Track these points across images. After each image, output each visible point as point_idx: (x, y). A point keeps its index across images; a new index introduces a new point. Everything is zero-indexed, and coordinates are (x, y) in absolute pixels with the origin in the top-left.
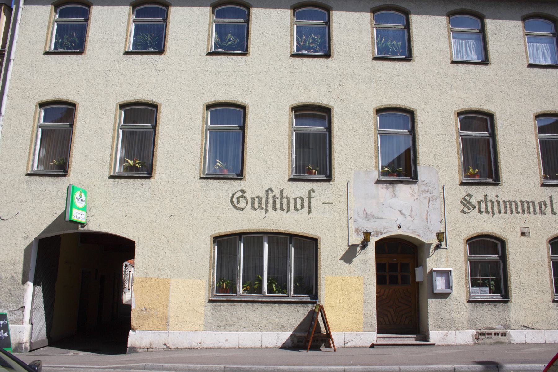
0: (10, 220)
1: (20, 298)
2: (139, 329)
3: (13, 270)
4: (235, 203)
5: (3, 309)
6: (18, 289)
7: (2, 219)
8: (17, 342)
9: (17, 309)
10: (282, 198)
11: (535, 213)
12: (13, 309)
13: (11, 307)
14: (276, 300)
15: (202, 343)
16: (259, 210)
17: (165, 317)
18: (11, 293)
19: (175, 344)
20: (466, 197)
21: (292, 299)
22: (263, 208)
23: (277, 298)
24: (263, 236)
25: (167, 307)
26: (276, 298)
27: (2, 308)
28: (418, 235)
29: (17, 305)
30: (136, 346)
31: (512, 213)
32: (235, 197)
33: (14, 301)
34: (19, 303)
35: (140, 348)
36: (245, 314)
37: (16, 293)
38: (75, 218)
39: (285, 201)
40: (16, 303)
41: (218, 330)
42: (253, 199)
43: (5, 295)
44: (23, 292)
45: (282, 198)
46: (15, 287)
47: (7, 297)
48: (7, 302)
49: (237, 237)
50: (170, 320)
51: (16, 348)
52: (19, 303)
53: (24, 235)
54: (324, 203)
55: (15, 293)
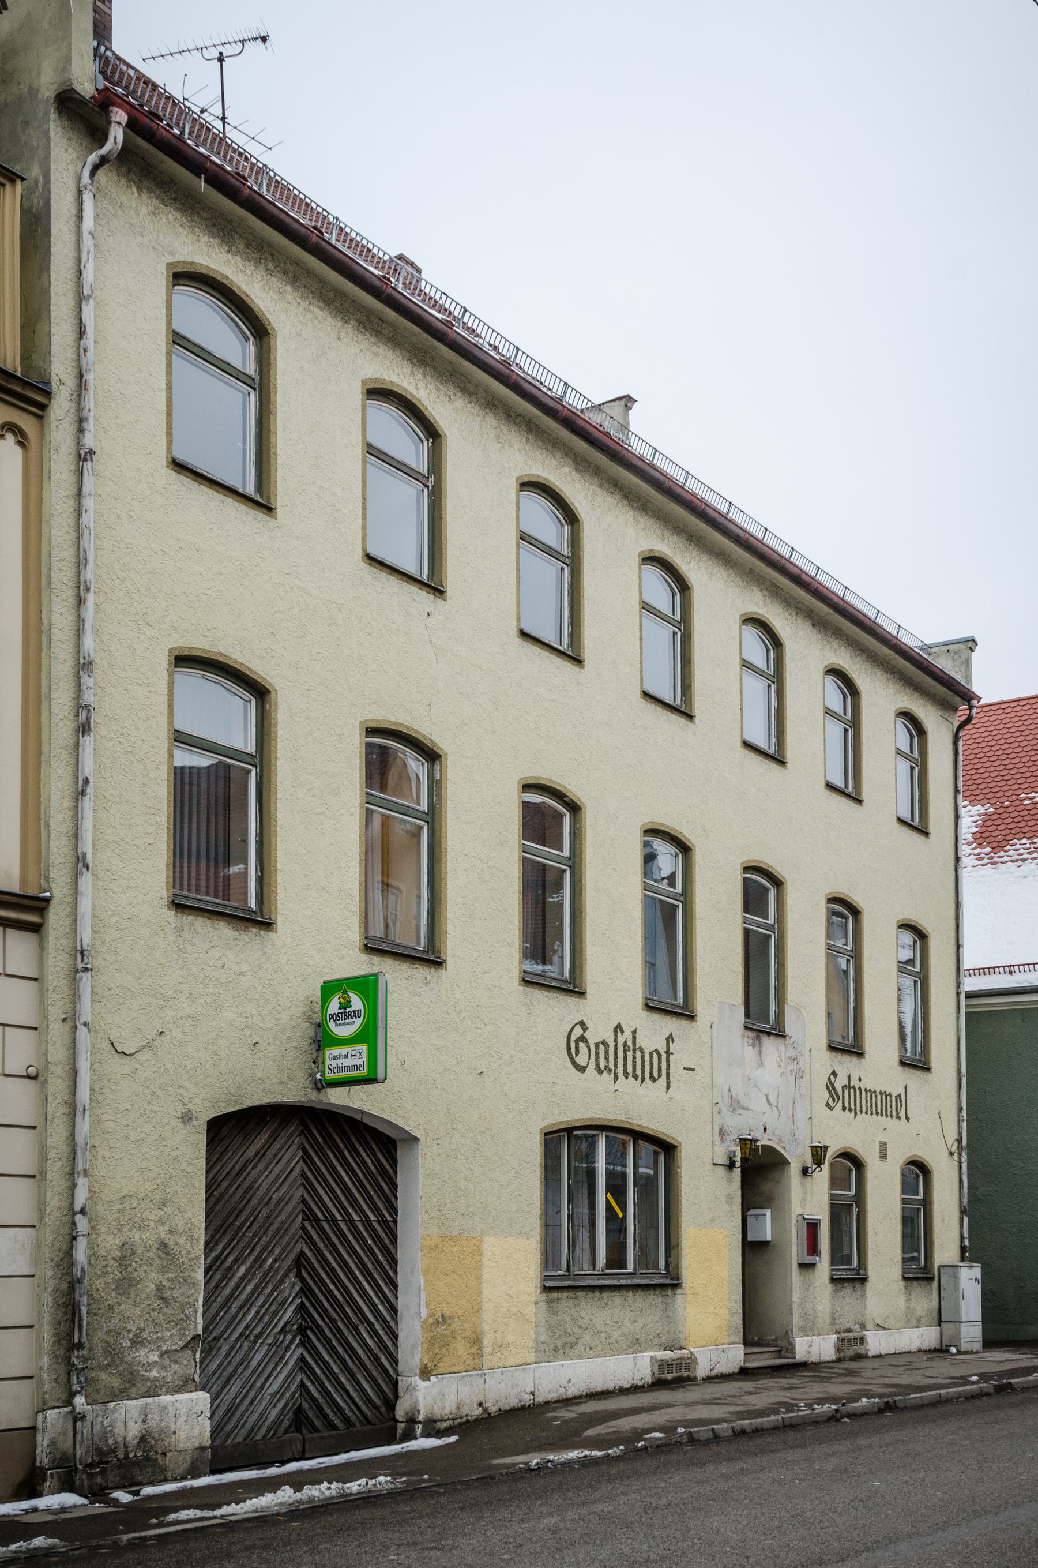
0: (139, 1056)
1: (187, 1311)
2: (434, 1373)
3: (160, 1222)
4: (574, 1054)
5: (146, 1350)
6: (179, 1281)
7: (119, 1050)
8: (197, 1445)
9: (181, 1344)
10: (634, 1050)
11: (892, 1117)
12: (174, 1348)
13: (166, 1340)
14: (623, 1282)
15: (537, 1393)
16: (605, 1073)
17: (475, 1337)
18: (165, 1296)
19: (497, 1401)
20: (242, 866)
21: (641, 1279)
22: (610, 1071)
23: (626, 1278)
24: (594, 1136)
25: (478, 1311)
26: (623, 1278)
27: (145, 1346)
28: (784, 1148)
29: (182, 1332)
30: (435, 1417)
31: (872, 1113)
32: (573, 1038)
33: (173, 1321)
34: (185, 1325)
35: (442, 1420)
36: (592, 1317)
37: (176, 1294)
38: (332, 1074)
39: (638, 1054)
40: (178, 1327)
41: (555, 1358)
42: (597, 1046)
43: (149, 1302)
44: (193, 1291)
45: (634, 1050)
46: (172, 1275)
47: (154, 1310)
48: (156, 1324)
49: (564, 1136)
50: (486, 1342)
51: (193, 1463)
52: (185, 1325)
53: (180, 1109)
54: (685, 1069)
55: (175, 1296)
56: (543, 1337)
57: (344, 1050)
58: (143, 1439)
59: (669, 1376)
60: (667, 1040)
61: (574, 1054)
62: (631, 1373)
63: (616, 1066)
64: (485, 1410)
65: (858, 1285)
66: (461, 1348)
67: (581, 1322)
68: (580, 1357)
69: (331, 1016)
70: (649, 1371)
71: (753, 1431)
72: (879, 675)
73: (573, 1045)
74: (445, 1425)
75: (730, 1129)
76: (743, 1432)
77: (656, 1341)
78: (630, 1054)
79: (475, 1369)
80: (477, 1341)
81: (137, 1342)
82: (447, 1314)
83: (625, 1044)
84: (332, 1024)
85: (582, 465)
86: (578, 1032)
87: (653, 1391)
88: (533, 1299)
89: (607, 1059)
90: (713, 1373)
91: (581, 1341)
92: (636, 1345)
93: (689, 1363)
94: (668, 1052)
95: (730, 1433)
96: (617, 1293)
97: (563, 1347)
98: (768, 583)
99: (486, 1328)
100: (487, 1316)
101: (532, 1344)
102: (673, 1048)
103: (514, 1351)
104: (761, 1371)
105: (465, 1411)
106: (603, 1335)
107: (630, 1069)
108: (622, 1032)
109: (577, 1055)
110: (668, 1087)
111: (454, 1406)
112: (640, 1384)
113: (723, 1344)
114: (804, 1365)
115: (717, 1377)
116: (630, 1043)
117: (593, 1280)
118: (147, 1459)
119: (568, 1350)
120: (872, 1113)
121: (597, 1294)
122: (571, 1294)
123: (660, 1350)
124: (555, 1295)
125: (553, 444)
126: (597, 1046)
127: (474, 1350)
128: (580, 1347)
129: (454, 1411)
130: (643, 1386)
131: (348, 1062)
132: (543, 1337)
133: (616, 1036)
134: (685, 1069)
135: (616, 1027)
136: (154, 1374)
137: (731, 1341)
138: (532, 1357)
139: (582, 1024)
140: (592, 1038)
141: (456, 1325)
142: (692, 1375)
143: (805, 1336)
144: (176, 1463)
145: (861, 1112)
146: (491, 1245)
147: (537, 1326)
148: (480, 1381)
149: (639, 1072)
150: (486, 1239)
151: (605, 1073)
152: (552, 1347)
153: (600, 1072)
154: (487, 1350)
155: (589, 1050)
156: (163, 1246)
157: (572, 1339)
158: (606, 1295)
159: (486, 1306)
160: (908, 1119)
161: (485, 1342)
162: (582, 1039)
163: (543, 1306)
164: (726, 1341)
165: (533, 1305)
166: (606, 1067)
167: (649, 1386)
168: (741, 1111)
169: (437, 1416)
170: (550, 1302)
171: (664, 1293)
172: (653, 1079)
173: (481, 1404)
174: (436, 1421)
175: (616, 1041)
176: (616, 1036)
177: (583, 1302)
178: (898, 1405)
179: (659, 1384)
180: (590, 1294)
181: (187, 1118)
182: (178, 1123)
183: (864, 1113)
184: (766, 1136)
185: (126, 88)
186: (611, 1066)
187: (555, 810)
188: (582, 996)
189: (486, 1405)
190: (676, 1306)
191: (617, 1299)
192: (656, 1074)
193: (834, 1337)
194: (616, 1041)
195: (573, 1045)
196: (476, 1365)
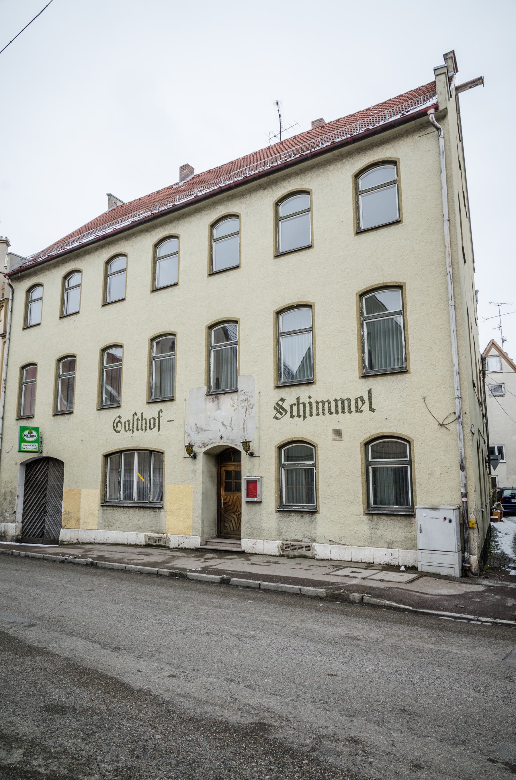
3: (10, 486)
10: (142, 420)
16: (128, 431)
22: (130, 430)
28: (236, 445)
35: (65, 542)
54: (168, 421)
56: (101, 521)
57: (29, 444)
58: (4, 532)
59: (154, 544)
60: (133, 415)
61: (115, 427)
62: (135, 539)
63: (133, 428)
64: (78, 541)
65: (307, 517)
66: (73, 521)
67: (115, 518)
68: (114, 530)
69: (25, 435)
70: (144, 540)
71: (32, 557)
72: (169, 228)
73: (115, 425)
74: (66, 543)
75: (196, 441)
76: (28, 556)
77: (150, 529)
78: (140, 423)
79: (77, 529)
80: (78, 520)
81: (6, 511)
82: (70, 511)
83: (138, 419)
84: (25, 437)
85: (162, 224)
86: (118, 419)
87: (144, 548)
88: (97, 509)
89: (129, 426)
90: (180, 547)
91: (115, 525)
92: (139, 529)
93: (166, 540)
94: (159, 417)
95: (24, 555)
96: (131, 509)
97: (108, 526)
98: (226, 199)
99: (81, 517)
100: (82, 513)
101: (96, 523)
102: (161, 414)
103: (90, 525)
104: (203, 550)
105: (72, 540)
106: (124, 524)
107: (139, 427)
108: (136, 415)
109: (117, 427)
110: (159, 430)
111: (69, 538)
112: (139, 544)
113: (189, 535)
114: (243, 552)
115: (182, 548)
116: (140, 418)
117: (127, 504)
118: (5, 536)
119: (110, 527)
120: (324, 414)
121: (122, 509)
122: (111, 508)
123: (152, 533)
124: (105, 508)
125: (155, 227)
126: (125, 423)
127: (77, 523)
128: (115, 527)
129: (69, 540)
130: (141, 545)
131: (31, 447)
132: (101, 521)
133: (134, 417)
134: (168, 421)
135: (159, 411)
136: (8, 518)
137: (193, 534)
138: (96, 527)
139: (120, 417)
140: (123, 420)
141: (72, 515)
142: (167, 545)
143: (251, 538)
144: (9, 538)
145: (311, 415)
146: (84, 492)
147: (98, 518)
148: (77, 532)
149: (144, 428)
150: (83, 490)
151: (128, 431)
152: (104, 525)
153: (126, 431)
154: (81, 523)
155: (122, 425)
156: (11, 491)
157: (112, 524)
158: (126, 509)
159: (81, 510)
160: (372, 409)
161: (81, 521)
162: (119, 422)
163: (101, 511)
164: (191, 534)
165: (97, 511)
166: (129, 429)
167: (144, 546)
168: (203, 432)
169: (64, 540)
170: (104, 510)
171: (154, 511)
172: (150, 428)
173: (77, 539)
174: (63, 541)
175: (133, 419)
176: (134, 417)
177: (116, 511)
178: (98, 565)
179: (148, 546)
180: (119, 509)
181: (16, 464)
182: (14, 465)
183: (140, 431)
184: (222, 441)
185: (308, 149)
186: (131, 428)
187: (73, 360)
188: (407, 372)
189: (79, 540)
190: (161, 516)
191: (131, 511)
192: (152, 427)
193: (279, 543)
194: (133, 419)
195: (115, 425)
196: (77, 527)
